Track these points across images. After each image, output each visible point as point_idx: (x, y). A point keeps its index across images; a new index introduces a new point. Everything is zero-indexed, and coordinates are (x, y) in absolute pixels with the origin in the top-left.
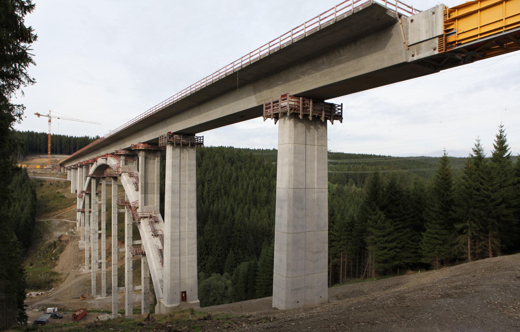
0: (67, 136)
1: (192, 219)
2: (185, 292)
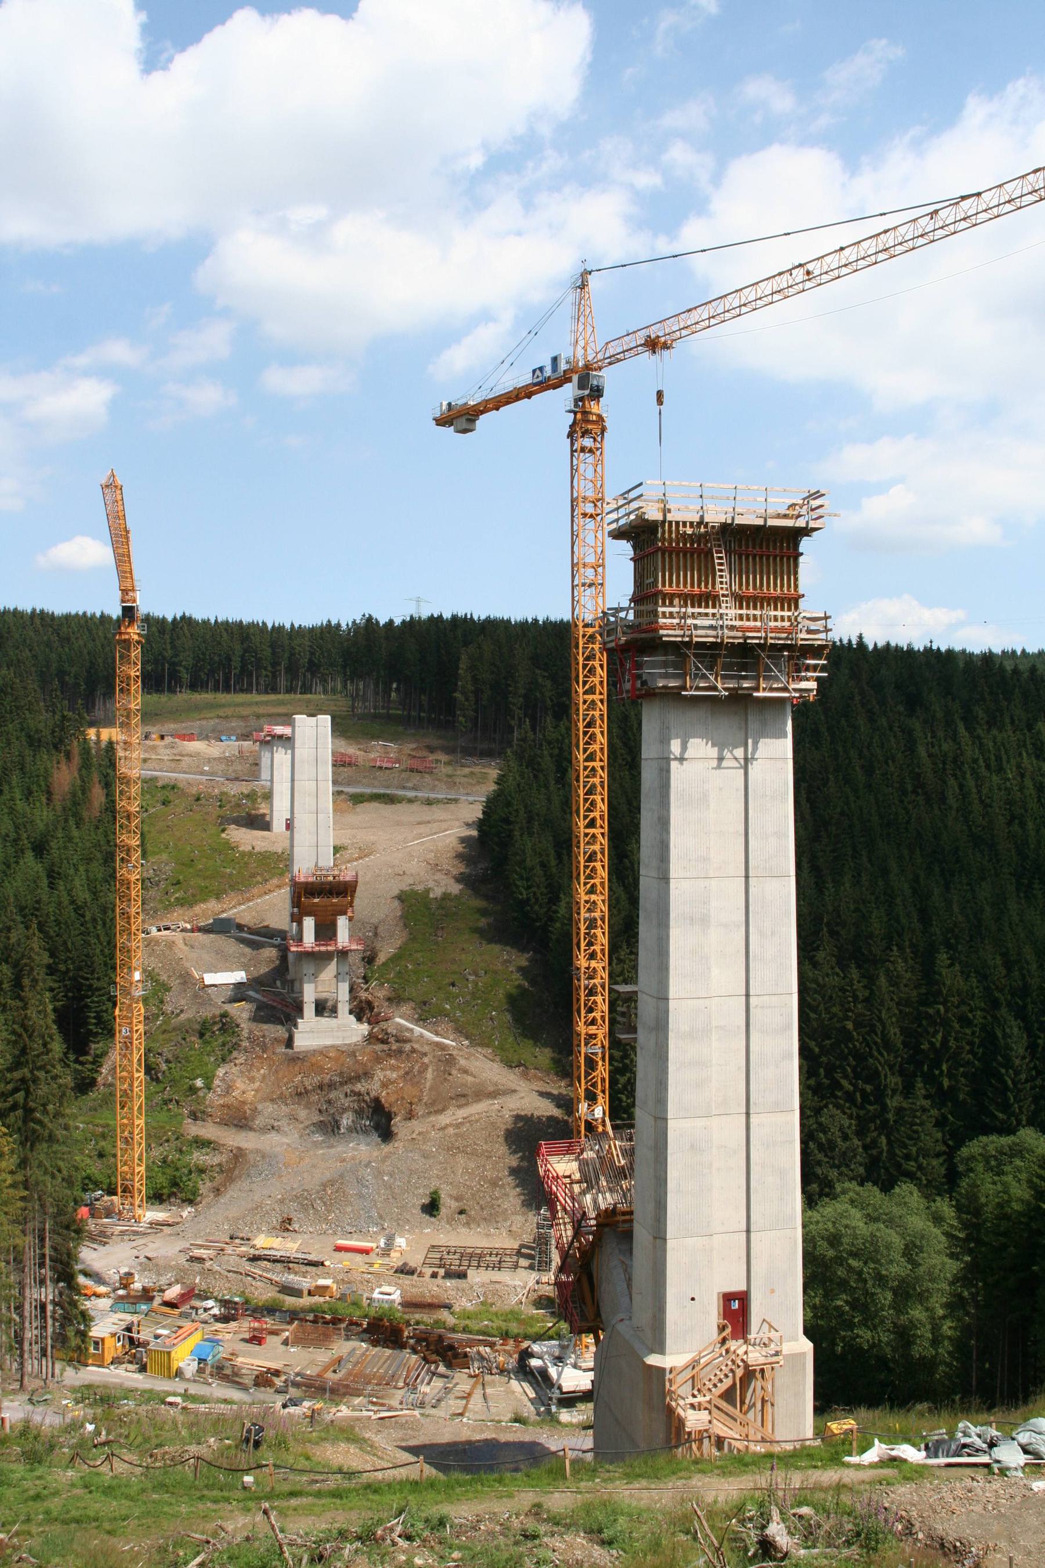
0: (264, 623)
1: (773, 933)
2: (743, 1298)
